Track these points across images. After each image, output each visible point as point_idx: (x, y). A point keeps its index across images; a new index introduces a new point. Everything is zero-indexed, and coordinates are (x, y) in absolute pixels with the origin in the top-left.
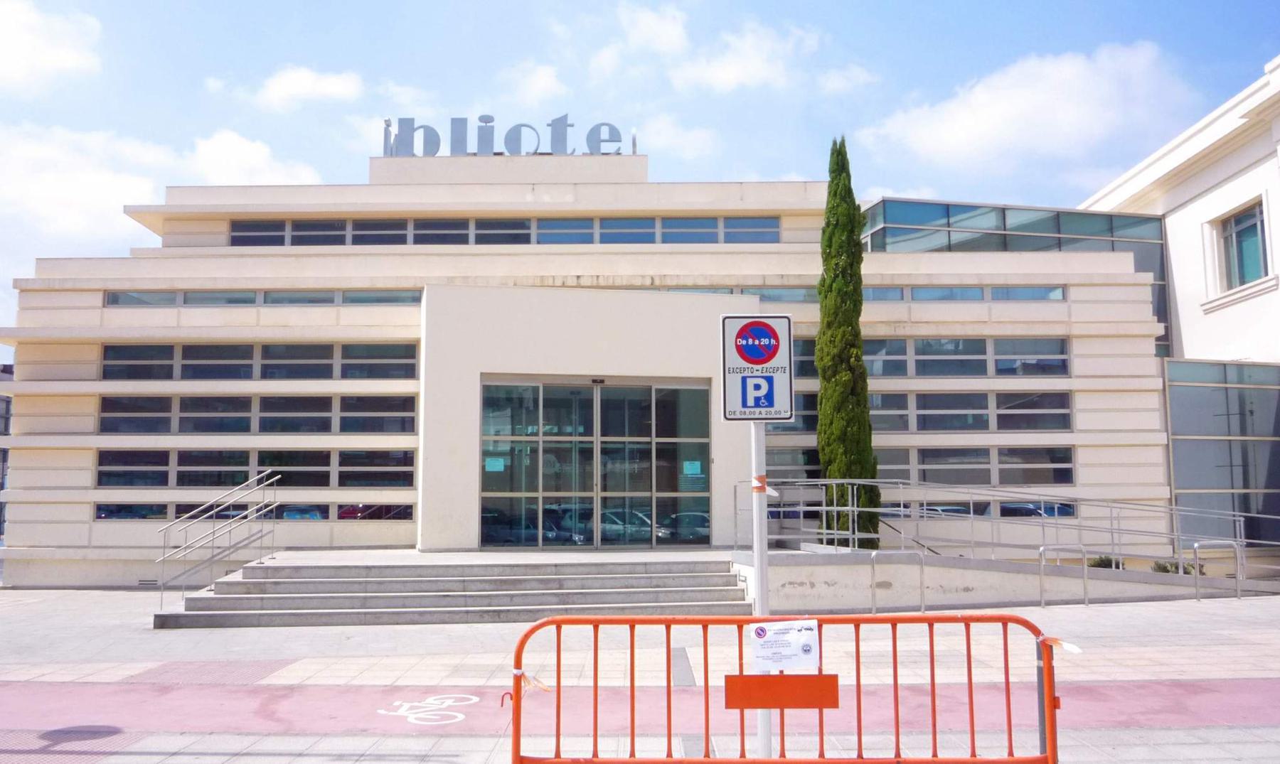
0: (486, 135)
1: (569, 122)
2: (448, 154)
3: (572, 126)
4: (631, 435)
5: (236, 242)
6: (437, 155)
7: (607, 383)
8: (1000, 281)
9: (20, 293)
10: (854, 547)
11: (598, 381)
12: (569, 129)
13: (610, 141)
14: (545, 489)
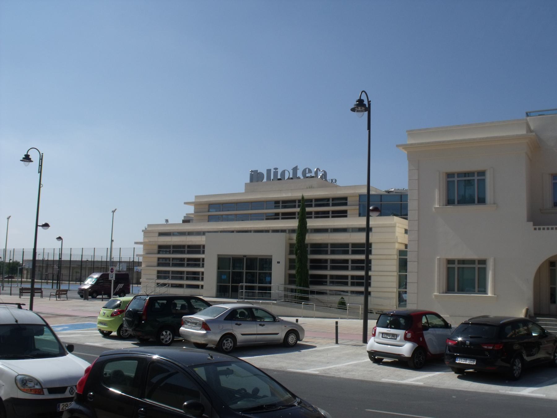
0: (276, 173)
1: (298, 168)
2: (266, 181)
3: (299, 169)
5: (345, 199)
7: (247, 257)
8: (292, 228)
9: (144, 233)
10: (340, 300)
11: (245, 256)
12: (298, 170)
14: (454, 268)
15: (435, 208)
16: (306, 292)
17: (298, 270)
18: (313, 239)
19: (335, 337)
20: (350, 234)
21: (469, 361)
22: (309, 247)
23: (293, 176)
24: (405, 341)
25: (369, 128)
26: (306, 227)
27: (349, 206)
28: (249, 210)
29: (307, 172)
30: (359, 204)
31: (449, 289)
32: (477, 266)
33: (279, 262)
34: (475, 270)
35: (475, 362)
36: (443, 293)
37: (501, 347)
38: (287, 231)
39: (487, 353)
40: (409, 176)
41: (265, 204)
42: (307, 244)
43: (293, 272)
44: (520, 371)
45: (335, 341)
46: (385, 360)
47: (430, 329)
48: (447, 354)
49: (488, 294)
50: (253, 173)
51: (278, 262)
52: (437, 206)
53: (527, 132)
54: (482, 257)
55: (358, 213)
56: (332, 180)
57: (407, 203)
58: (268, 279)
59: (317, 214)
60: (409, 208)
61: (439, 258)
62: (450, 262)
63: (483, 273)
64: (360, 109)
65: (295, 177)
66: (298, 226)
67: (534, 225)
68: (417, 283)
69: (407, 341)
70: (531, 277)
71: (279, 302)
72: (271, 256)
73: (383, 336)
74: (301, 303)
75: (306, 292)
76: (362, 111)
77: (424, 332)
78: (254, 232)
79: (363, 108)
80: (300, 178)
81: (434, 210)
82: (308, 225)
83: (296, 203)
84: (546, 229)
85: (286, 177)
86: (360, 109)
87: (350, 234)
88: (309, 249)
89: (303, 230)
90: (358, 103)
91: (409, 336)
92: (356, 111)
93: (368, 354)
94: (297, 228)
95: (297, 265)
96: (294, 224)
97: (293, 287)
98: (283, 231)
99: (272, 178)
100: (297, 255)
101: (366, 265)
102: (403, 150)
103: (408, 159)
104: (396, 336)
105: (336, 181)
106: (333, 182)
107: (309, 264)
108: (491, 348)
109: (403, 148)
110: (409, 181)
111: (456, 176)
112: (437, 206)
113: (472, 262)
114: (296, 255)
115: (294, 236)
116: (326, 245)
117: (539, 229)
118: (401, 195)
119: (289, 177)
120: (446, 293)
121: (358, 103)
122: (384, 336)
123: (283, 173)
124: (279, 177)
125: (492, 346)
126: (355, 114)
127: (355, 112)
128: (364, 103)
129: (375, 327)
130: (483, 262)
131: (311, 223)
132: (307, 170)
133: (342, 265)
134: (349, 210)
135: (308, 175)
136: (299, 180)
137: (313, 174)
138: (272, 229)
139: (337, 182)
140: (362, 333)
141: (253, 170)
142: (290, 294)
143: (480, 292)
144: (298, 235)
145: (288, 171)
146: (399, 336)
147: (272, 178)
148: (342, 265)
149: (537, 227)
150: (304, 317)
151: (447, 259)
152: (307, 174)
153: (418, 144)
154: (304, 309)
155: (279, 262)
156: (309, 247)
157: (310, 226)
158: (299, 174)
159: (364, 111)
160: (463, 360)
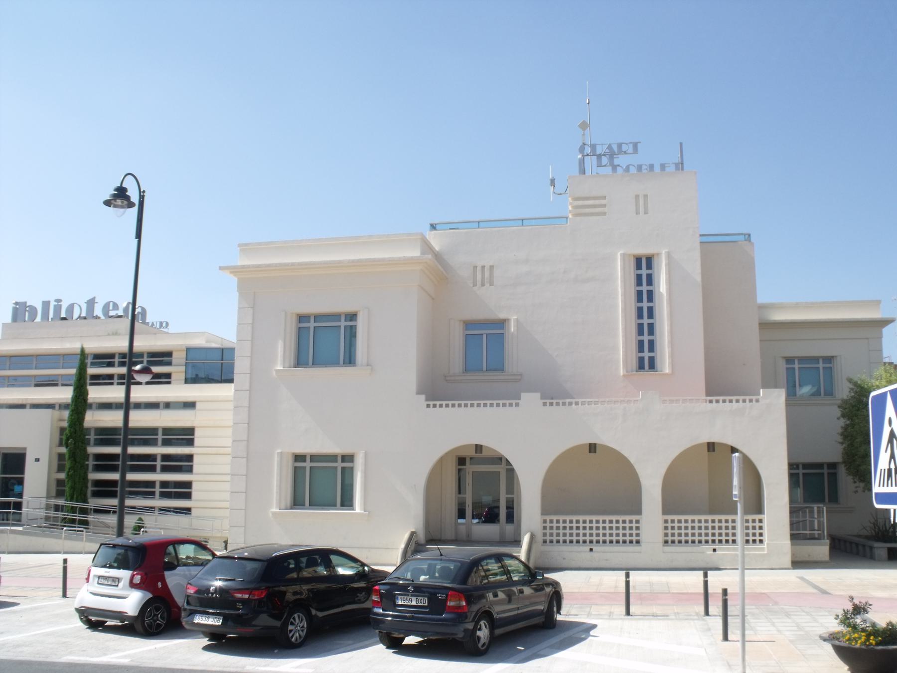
0: (58, 308)
1: (96, 301)
3: (97, 303)
4: (76, 519)
5: (169, 354)
6: (35, 321)
10: (136, 523)
12: (95, 304)
13: (113, 310)
14: (305, 468)
15: (278, 371)
16: (84, 511)
17: (69, 472)
18: (99, 421)
19: (61, 585)
20: (93, 413)
21: (212, 620)
22: (92, 432)
23: (86, 315)
24: (130, 589)
25: (139, 235)
26: (85, 399)
27: (175, 366)
28: (58, 368)
29: (111, 308)
30: (186, 363)
31: (297, 502)
32: (339, 465)
33: (37, 460)
34: (337, 471)
35: (221, 621)
36: (286, 509)
37: (263, 596)
38: (57, 407)
39: (239, 605)
40: (239, 318)
41: (34, 359)
42: (89, 429)
43: (62, 476)
44: (303, 634)
45: (61, 593)
46: (110, 623)
47: (179, 568)
48: (185, 610)
49: (355, 510)
50: (18, 306)
51: (36, 459)
52: (279, 367)
53: (423, 253)
54: (347, 451)
55: (184, 378)
56: (161, 323)
57: (234, 363)
58: (17, 489)
59: (121, 379)
60: (236, 370)
61: (281, 452)
62: (299, 458)
63: (347, 475)
64: (120, 203)
65: (90, 315)
66: (72, 398)
67: (427, 400)
68: (245, 492)
69: (133, 589)
70: (421, 481)
71: (28, 529)
72: (25, 449)
73: (100, 582)
74: (63, 529)
75: (84, 511)
76: (122, 207)
77: (166, 573)
78: (30, 408)
79: (126, 202)
80: (99, 318)
81: (274, 373)
82: (90, 396)
83: (143, 358)
84: (450, 405)
85: (76, 316)
86: (120, 203)
87: (93, 413)
88: (92, 437)
89: (80, 404)
90: (116, 192)
91: (137, 580)
92: (112, 206)
93: (77, 615)
94: (69, 401)
95: (68, 464)
96: (66, 394)
97: (61, 502)
98: (50, 406)
99: (51, 315)
100: (69, 447)
101: (184, 463)
102: (232, 276)
103: (238, 291)
104: (117, 580)
105: (167, 324)
106: (162, 326)
107: (91, 463)
108: (247, 596)
109: (231, 273)
110: (237, 326)
111: (312, 319)
112: (279, 367)
113: (332, 458)
114: (67, 447)
115: (66, 414)
116: (153, 431)
117: (435, 406)
118: (223, 349)
119: (80, 315)
120: (291, 508)
121: (116, 192)
122: (101, 581)
123: (71, 308)
124: (63, 315)
125: (247, 594)
126: (111, 210)
127: (110, 207)
128: (127, 194)
129: (90, 567)
130: (348, 458)
131: (95, 394)
132: (111, 304)
133: (146, 463)
134: (174, 372)
135: (112, 313)
136: (98, 320)
137: (120, 313)
138: (30, 402)
139: (169, 327)
140: (62, 577)
141: (18, 301)
142: (52, 513)
143: (343, 505)
144: (71, 413)
145: (80, 306)
146: (122, 580)
147: (51, 315)
148: (146, 463)
149: (431, 403)
150: (9, 553)
151: (293, 453)
152: (110, 312)
153: (253, 266)
154: (66, 538)
155: (37, 460)
156: (92, 432)
157: (135, 397)
158: (98, 311)
159: (126, 206)
160: (204, 618)
